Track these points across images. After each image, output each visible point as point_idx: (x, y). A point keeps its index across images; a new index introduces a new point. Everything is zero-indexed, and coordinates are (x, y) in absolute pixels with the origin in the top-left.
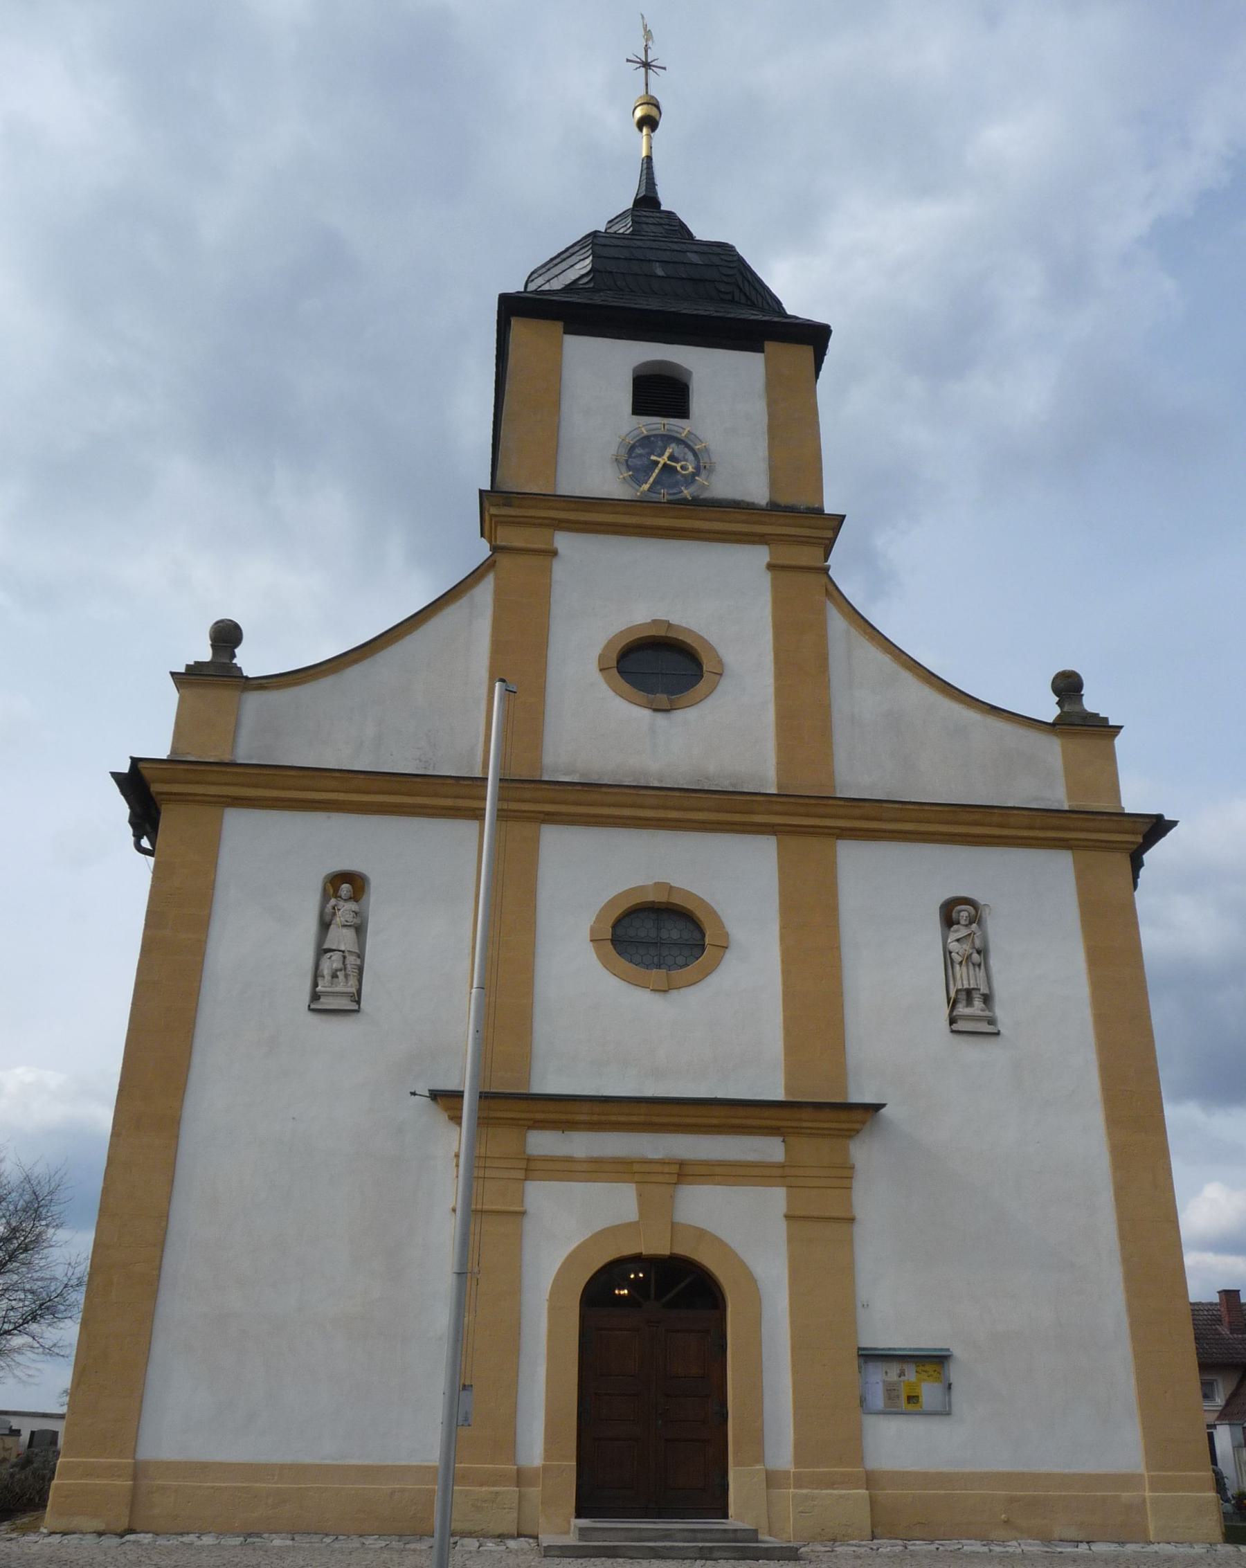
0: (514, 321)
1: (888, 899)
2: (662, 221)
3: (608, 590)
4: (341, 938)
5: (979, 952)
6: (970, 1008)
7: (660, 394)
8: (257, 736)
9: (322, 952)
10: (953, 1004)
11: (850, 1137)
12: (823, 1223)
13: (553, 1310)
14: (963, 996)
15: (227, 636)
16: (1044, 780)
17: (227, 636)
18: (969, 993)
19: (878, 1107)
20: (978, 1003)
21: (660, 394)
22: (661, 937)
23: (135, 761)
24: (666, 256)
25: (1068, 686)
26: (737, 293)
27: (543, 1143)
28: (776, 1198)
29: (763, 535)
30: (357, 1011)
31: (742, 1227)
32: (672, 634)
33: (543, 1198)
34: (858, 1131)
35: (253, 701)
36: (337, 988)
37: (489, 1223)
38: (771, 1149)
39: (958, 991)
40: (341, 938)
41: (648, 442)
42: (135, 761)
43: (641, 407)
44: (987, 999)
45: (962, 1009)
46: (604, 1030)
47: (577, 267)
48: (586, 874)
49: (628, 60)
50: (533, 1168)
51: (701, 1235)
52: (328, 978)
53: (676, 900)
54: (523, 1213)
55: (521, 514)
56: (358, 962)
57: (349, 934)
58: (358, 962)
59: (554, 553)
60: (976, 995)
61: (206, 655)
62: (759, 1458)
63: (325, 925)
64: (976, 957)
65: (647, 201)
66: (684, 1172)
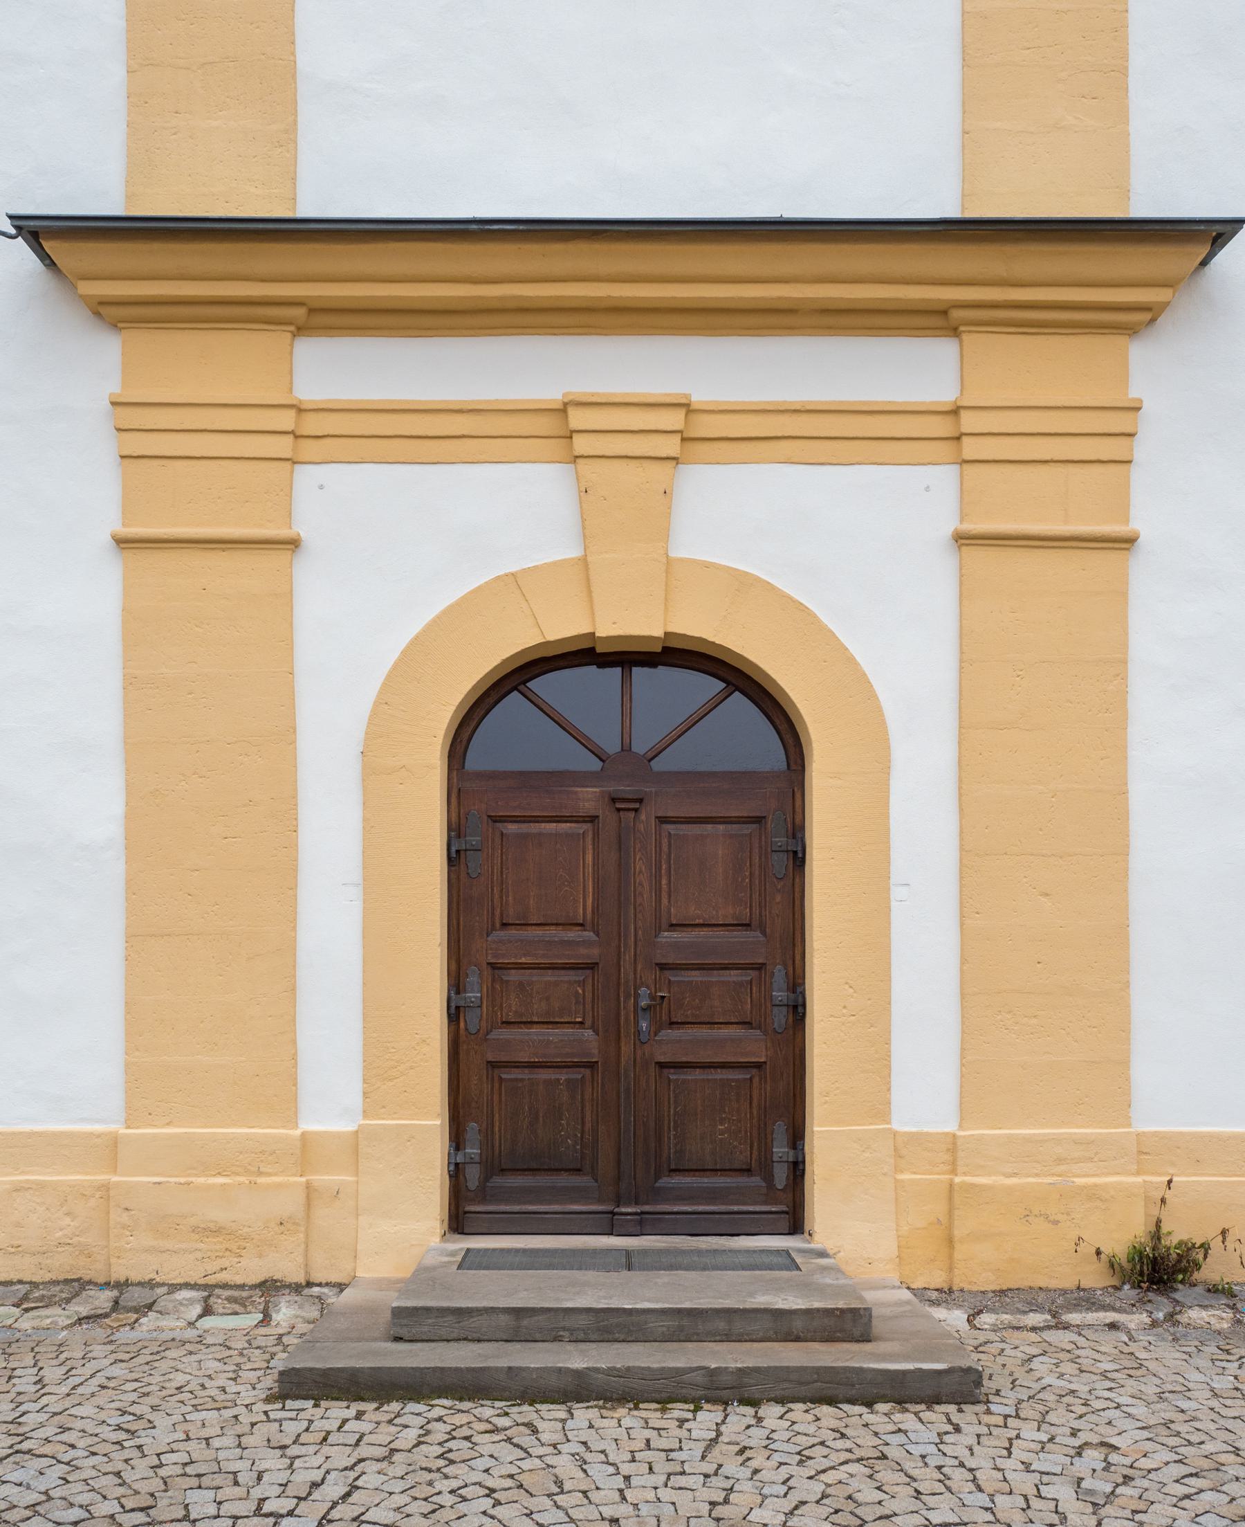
11: (1131, 331)
12: (1051, 555)
13: (375, 768)
27: (333, 371)
28: (919, 501)
33: (331, 499)
37: (201, 559)
38: (917, 372)
50: (313, 434)
54: (1129, 541)
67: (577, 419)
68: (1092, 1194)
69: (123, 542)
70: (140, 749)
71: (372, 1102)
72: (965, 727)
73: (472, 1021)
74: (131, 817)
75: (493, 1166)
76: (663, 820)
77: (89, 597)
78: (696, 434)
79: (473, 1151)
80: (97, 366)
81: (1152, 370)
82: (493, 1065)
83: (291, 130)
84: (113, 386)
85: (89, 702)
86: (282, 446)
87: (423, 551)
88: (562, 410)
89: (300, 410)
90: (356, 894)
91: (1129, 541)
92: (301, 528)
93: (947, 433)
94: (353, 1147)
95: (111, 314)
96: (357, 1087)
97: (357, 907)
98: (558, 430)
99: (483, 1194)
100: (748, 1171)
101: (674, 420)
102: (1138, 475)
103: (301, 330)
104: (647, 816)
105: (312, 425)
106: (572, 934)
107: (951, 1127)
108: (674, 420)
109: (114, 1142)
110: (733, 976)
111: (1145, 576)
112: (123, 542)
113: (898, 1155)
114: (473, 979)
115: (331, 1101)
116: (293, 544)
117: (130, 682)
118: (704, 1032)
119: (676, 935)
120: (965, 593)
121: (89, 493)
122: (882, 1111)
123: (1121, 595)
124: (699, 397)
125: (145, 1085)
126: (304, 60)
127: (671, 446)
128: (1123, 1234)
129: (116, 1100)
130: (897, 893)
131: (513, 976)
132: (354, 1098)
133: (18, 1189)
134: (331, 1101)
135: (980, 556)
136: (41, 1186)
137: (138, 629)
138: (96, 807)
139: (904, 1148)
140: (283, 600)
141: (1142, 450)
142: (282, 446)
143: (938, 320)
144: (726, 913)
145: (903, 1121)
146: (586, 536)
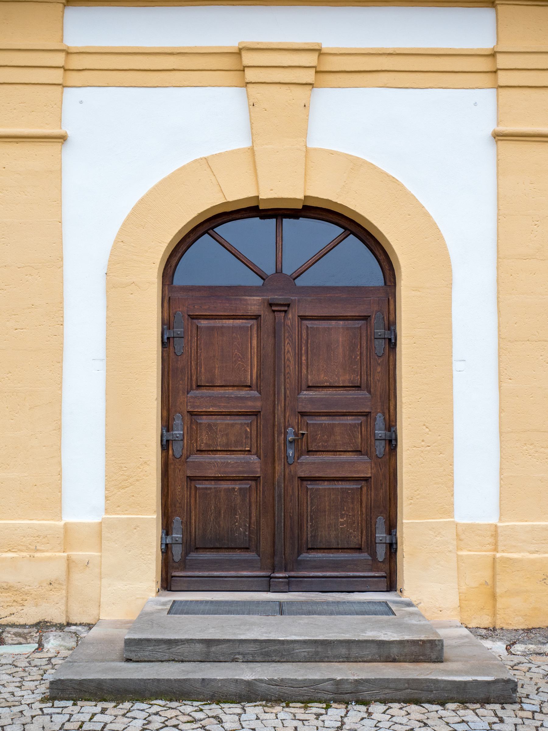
13: (115, 285)
28: (475, 110)
33: (85, 109)
50: (74, 68)
71: (111, 503)
73: (177, 449)
75: (191, 546)
76: (303, 318)
78: (323, 68)
79: (177, 535)
82: (191, 479)
86: (57, 76)
88: (238, 53)
89: (68, 53)
90: (101, 366)
91: (63, 138)
93: (489, 67)
94: (99, 532)
98: (236, 65)
100: (359, 549)
101: (311, 59)
104: (292, 315)
105: (76, 62)
106: (243, 393)
107: (494, 520)
110: (350, 420)
115: (84, 499)
119: (312, 394)
124: (327, 45)
127: (309, 76)
130: (457, 366)
131: (204, 420)
132: (101, 502)
135: (512, 149)
139: (463, 534)
140: (56, 174)
144: (344, 379)
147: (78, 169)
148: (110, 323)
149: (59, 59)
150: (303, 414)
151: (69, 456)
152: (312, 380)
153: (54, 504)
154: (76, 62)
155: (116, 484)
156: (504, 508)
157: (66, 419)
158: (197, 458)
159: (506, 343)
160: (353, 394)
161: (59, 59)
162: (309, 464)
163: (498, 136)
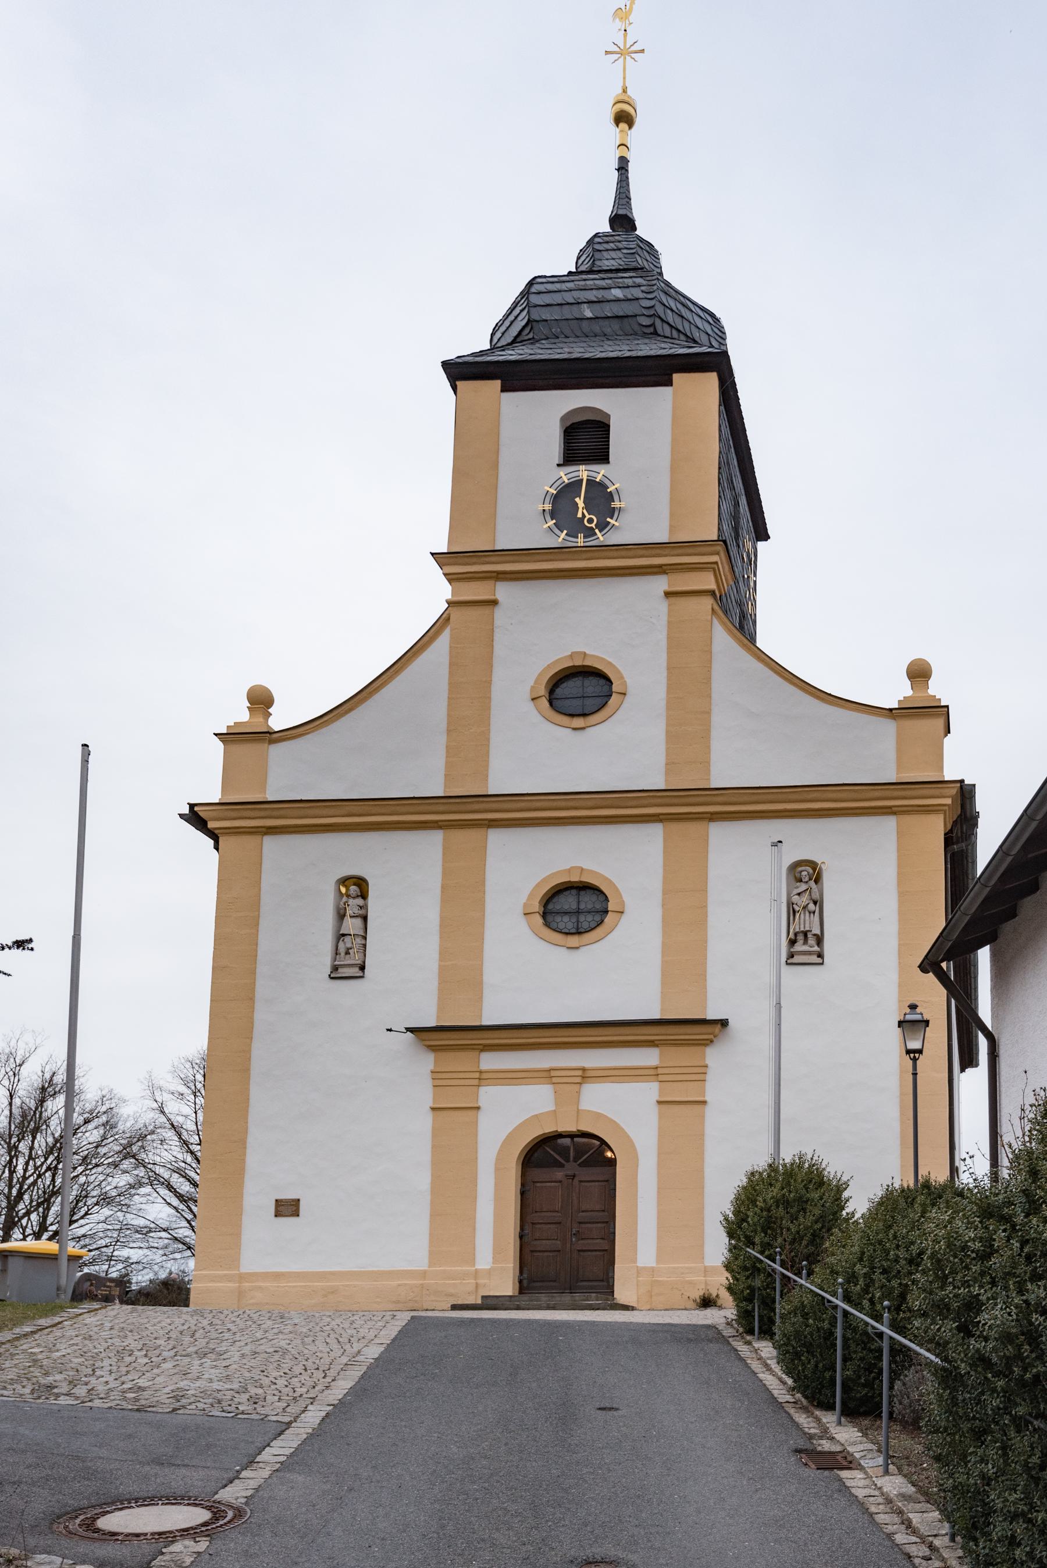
0: (458, 383)
1: (744, 866)
2: (620, 245)
3: (545, 626)
4: (352, 925)
5: (815, 903)
6: (804, 944)
7: (586, 440)
8: (286, 777)
9: (340, 936)
10: (792, 942)
11: (706, 1045)
12: (683, 1106)
13: (498, 1169)
14: (800, 937)
15: (261, 701)
16: (877, 759)
17: (261, 701)
18: (805, 934)
19: (724, 1023)
20: (812, 941)
21: (586, 440)
22: (574, 908)
23: (192, 806)
24: (591, 295)
25: (919, 673)
26: (658, 322)
27: (490, 1061)
28: (649, 1091)
29: (660, 566)
30: (362, 977)
31: (623, 1108)
32: (587, 663)
33: (489, 1095)
34: (712, 1041)
35: (276, 752)
36: (348, 963)
37: (454, 1113)
38: (649, 1057)
39: (796, 934)
40: (352, 925)
41: (571, 489)
42: (192, 806)
43: (570, 457)
44: (819, 940)
45: (799, 947)
46: (530, 977)
47: (520, 318)
48: (521, 865)
49: (607, 53)
50: (483, 1078)
51: (599, 1116)
52: (343, 954)
53: (587, 879)
54: (478, 1108)
55: (474, 566)
56: (363, 942)
57: (359, 922)
58: (363, 942)
59: (494, 603)
60: (809, 935)
61: (244, 716)
62: (634, 1260)
63: (341, 916)
64: (811, 906)
65: (622, 220)
66: (585, 1075)
67: (553, 1073)
68: (690, 1283)
69: (659, 1102)
70: (436, 1164)
71: (495, 1260)
72: (660, 1154)
73: (525, 1239)
74: (432, 1183)
75: (531, 1280)
76: (581, 1181)
77: (425, 1122)
78: (585, 1075)
79: (525, 1276)
80: (428, 1061)
81: (713, 1056)
82: (532, 1251)
83: (481, 998)
84: (431, 1067)
85: (423, 1153)
86: (476, 1082)
87: (514, 1109)
88: (550, 1070)
89: (481, 1072)
90: (492, 1203)
91: (478, 1108)
92: (480, 1104)
93: (653, 1073)
94: (489, 1273)
95: (432, 1048)
96: (491, 1256)
97: (492, 1207)
98: (547, 1075)
99: (528, 1288)
100: (602, 1281)
101: (579, 1073)
102: (708, 1084)
103: (482, 1051)
104: (576, 1180)
105: (484, 1076)
106: (554, 1214)
107: (654, 1265)
108: (579, 1073)
109: (425, 1272)
110: (599, 1225)
111: (709, 1111)
112: (659, 1102)
113: (638, 1272)
114: (526, 1227)
115: (484, 1260)
116: (704, 1102)
117: (434, 1147)
118: (590, 1241)
119: (584, 1214)
120: (661, 1116)
121: (424, 1095)
122: (635, 1261)
123: (703, 1117)
124: (587, 1065)
125: (435, 1255)
126: (485, 978)
127: (578, 1080)
128: (697, 1294)
129: (426, 1261)
130: (639, 1200)
131: (538, 1226)
132: (490, 1260)
133: (399, 1285)
134: (484, 1260)
135: (664, 1107)
136: (406, 1284)
137: (436, 1132)
138: (423, 1180)
139: (639, 1271)
140: (475, 1123)
141: (708, 1077)
142: (476, 1082)
143: (651, 1044)
144: (598, 1207)
145: (640, 1263)
146: (556, 1104)
147: (484, 1120)
148: (496, 1185)
149: (477, 1075)
150: (580, 1223)
151: (479, 1241)
152: (583, 1208)
153: (472, 1261)
154: (484, 1076)
155: (498, 1251)
156: (659, 1260)
157: (477, 1225)
158: (535, 1243)
159: (661, 1189)
160: (601, 1214)
161: (477, 1075)
162: (581, 1244)
163: (433, 1109)
